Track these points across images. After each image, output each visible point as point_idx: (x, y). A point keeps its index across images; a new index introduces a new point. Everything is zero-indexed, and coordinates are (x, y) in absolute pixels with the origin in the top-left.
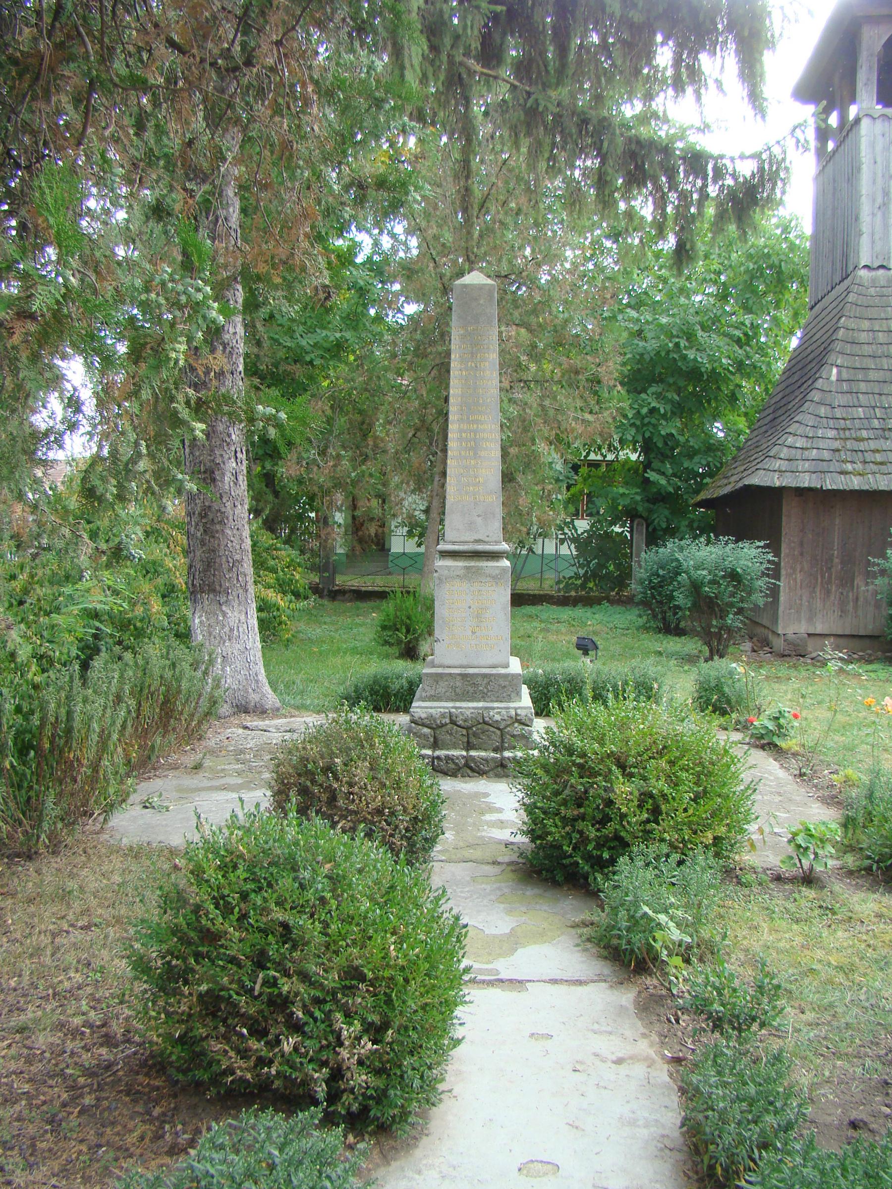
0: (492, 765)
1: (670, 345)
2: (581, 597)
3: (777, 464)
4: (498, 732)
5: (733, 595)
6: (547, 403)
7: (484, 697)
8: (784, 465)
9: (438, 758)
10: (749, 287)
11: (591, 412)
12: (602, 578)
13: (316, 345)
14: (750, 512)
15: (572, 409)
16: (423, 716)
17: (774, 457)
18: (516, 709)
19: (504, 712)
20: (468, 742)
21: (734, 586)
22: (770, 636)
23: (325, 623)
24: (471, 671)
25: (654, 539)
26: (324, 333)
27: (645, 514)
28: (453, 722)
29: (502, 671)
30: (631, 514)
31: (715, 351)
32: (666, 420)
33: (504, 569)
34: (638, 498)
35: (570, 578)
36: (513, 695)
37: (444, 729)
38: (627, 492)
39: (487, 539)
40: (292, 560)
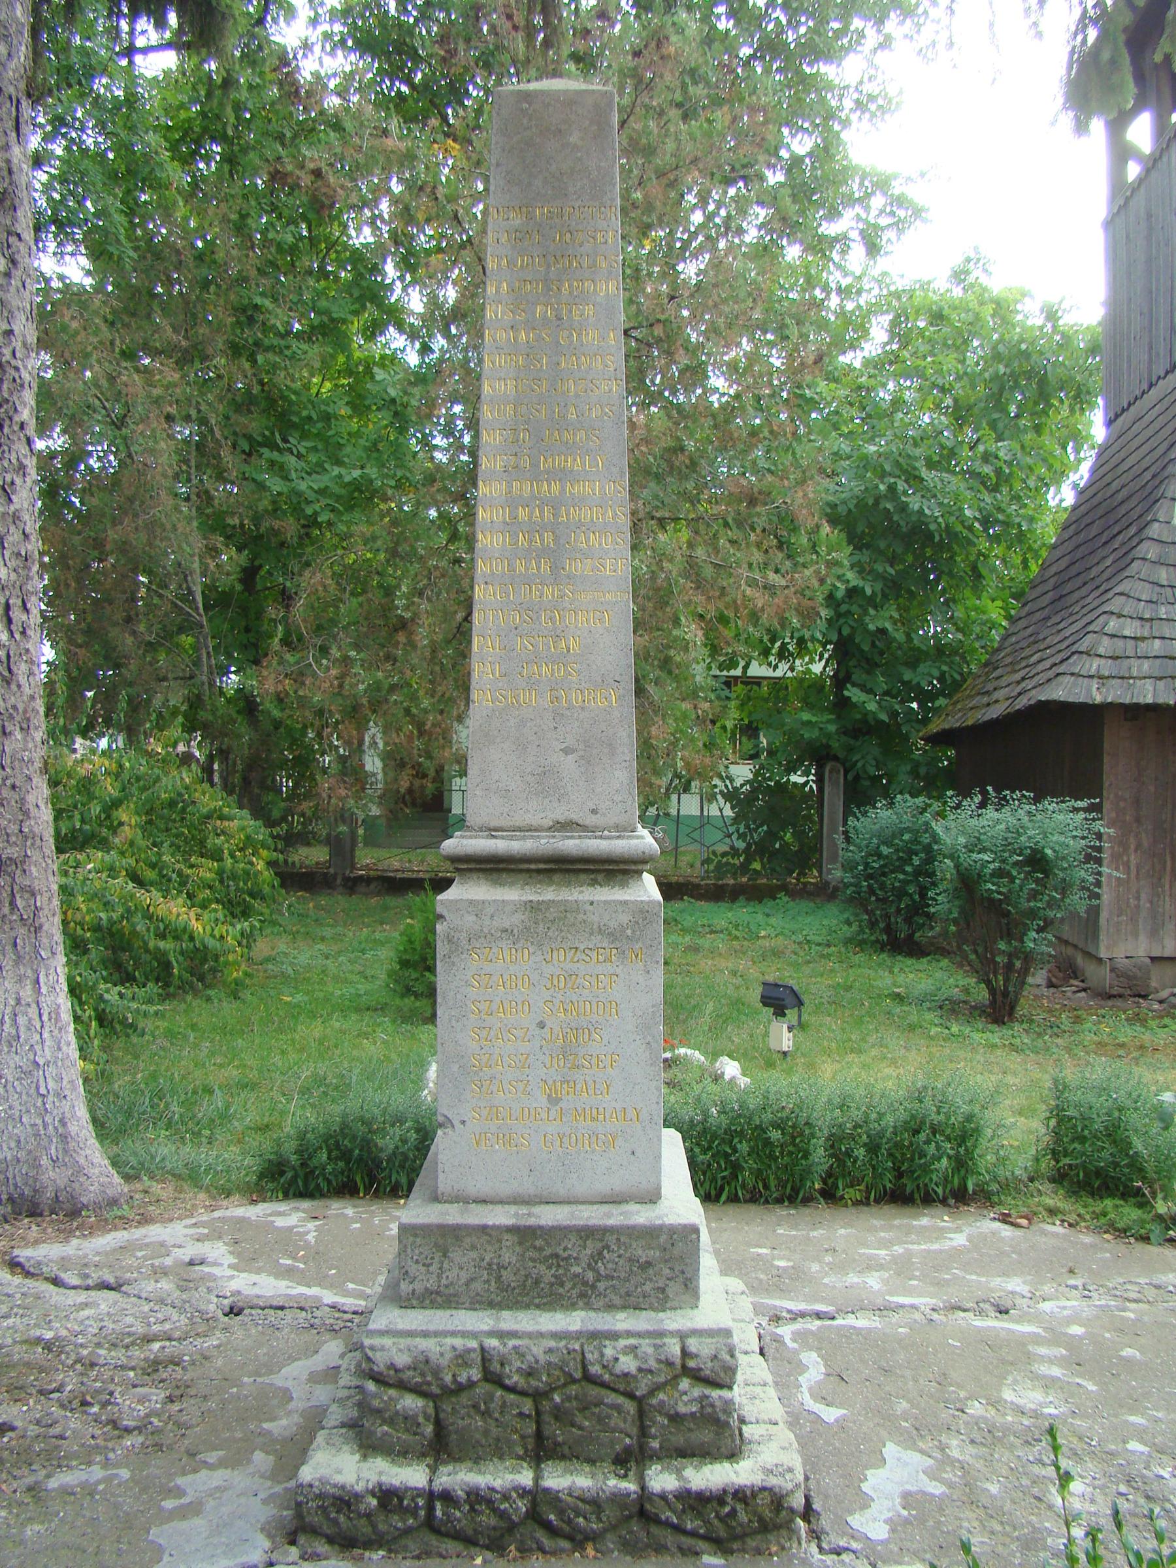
0: (610, 1514)
1: (882, 487)
2: (742, 885)
3: (1094, 665)
4: (630, 1407)
5: (1034, 895)
6: (700, 552)
7: (584, 1295)
8: (1107, 667)
9: (447, 1497)
10: (998, 400)
11: (777, 571)
12: (774, 854)
13: (322, 492)
14: (1048, 748)
15: (745, 566)
16: (402, 1360)
17: (1088, 653)
18: (682, 1336)
19: (646, 1346)
20: (539, 1435)
21: (1037, 881)
22: (1080, 960)
23: (323, 939)
24: (548, 1216)
25: (859, 795)
26: (336, 471)
27: (841, 754)
28: (493, 1378)
29: (641, 1216)
30: (818, 755)
31: (943, 498)
32: (875, 608)
33: (643, 910)
34: (832, 728)
35: (724, 854)
36: (673, 1289)
37: (464, 1399)
38: (814, 719)
39: (590, 820)
40: (248, 837)
